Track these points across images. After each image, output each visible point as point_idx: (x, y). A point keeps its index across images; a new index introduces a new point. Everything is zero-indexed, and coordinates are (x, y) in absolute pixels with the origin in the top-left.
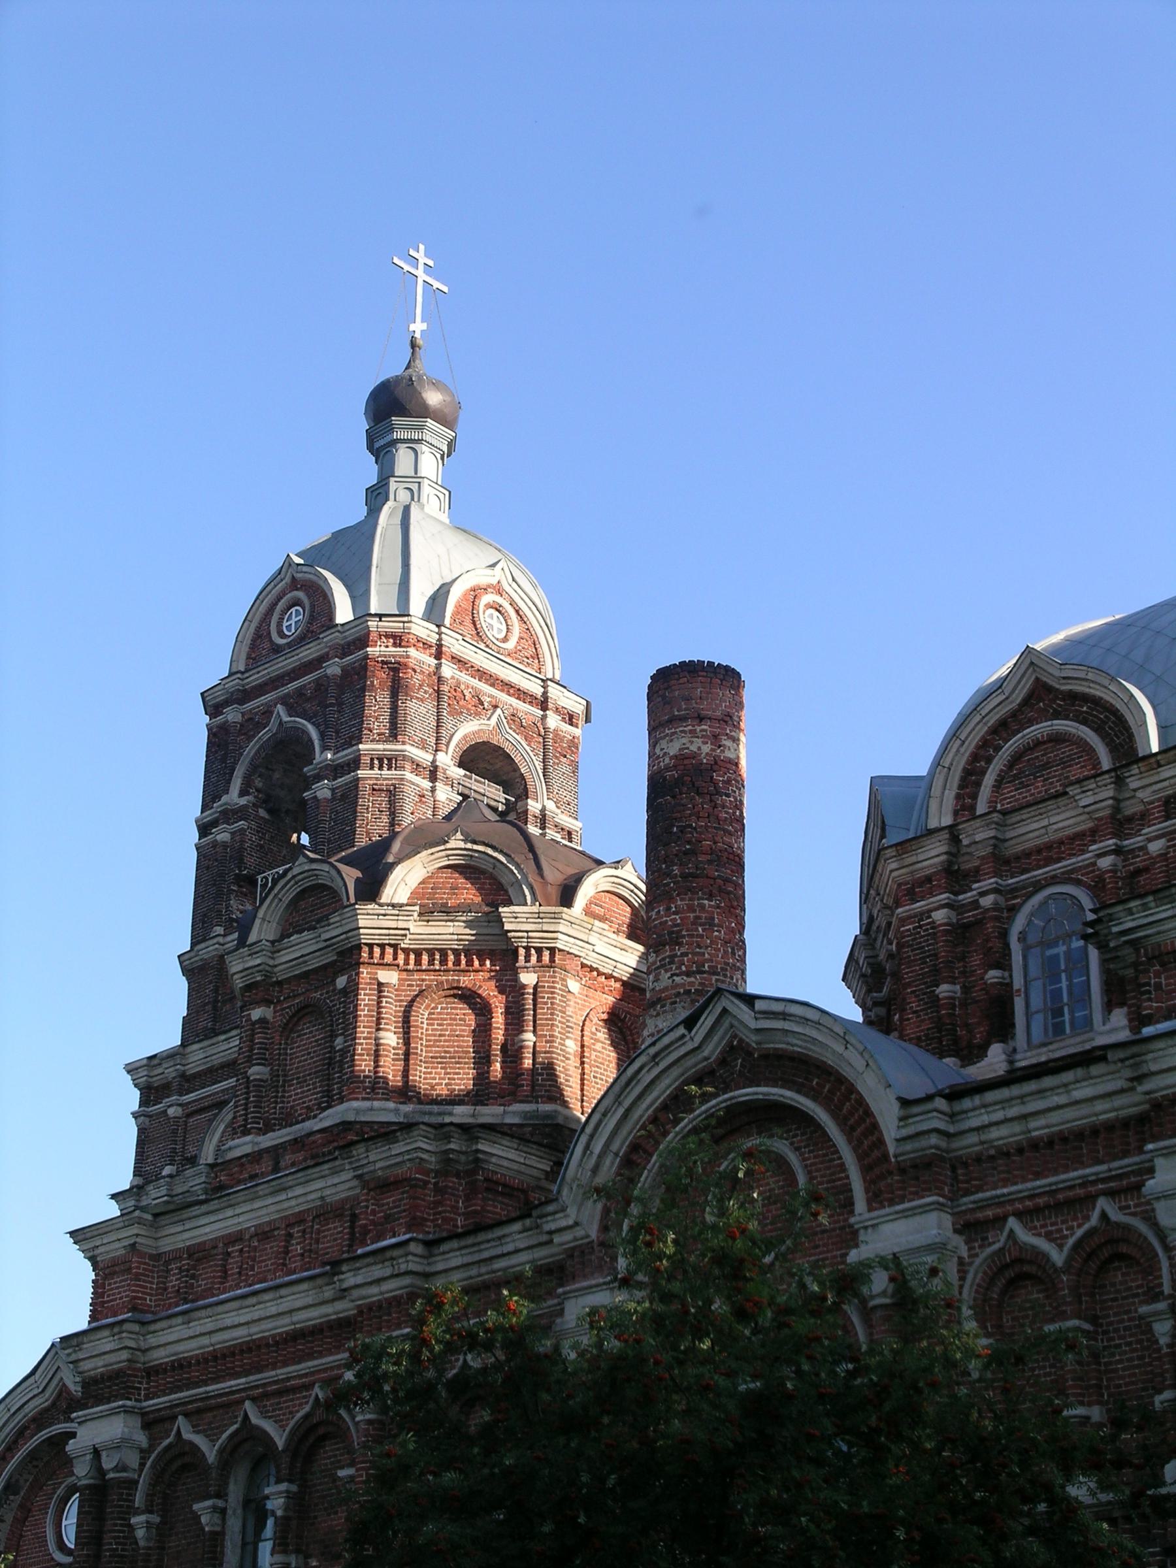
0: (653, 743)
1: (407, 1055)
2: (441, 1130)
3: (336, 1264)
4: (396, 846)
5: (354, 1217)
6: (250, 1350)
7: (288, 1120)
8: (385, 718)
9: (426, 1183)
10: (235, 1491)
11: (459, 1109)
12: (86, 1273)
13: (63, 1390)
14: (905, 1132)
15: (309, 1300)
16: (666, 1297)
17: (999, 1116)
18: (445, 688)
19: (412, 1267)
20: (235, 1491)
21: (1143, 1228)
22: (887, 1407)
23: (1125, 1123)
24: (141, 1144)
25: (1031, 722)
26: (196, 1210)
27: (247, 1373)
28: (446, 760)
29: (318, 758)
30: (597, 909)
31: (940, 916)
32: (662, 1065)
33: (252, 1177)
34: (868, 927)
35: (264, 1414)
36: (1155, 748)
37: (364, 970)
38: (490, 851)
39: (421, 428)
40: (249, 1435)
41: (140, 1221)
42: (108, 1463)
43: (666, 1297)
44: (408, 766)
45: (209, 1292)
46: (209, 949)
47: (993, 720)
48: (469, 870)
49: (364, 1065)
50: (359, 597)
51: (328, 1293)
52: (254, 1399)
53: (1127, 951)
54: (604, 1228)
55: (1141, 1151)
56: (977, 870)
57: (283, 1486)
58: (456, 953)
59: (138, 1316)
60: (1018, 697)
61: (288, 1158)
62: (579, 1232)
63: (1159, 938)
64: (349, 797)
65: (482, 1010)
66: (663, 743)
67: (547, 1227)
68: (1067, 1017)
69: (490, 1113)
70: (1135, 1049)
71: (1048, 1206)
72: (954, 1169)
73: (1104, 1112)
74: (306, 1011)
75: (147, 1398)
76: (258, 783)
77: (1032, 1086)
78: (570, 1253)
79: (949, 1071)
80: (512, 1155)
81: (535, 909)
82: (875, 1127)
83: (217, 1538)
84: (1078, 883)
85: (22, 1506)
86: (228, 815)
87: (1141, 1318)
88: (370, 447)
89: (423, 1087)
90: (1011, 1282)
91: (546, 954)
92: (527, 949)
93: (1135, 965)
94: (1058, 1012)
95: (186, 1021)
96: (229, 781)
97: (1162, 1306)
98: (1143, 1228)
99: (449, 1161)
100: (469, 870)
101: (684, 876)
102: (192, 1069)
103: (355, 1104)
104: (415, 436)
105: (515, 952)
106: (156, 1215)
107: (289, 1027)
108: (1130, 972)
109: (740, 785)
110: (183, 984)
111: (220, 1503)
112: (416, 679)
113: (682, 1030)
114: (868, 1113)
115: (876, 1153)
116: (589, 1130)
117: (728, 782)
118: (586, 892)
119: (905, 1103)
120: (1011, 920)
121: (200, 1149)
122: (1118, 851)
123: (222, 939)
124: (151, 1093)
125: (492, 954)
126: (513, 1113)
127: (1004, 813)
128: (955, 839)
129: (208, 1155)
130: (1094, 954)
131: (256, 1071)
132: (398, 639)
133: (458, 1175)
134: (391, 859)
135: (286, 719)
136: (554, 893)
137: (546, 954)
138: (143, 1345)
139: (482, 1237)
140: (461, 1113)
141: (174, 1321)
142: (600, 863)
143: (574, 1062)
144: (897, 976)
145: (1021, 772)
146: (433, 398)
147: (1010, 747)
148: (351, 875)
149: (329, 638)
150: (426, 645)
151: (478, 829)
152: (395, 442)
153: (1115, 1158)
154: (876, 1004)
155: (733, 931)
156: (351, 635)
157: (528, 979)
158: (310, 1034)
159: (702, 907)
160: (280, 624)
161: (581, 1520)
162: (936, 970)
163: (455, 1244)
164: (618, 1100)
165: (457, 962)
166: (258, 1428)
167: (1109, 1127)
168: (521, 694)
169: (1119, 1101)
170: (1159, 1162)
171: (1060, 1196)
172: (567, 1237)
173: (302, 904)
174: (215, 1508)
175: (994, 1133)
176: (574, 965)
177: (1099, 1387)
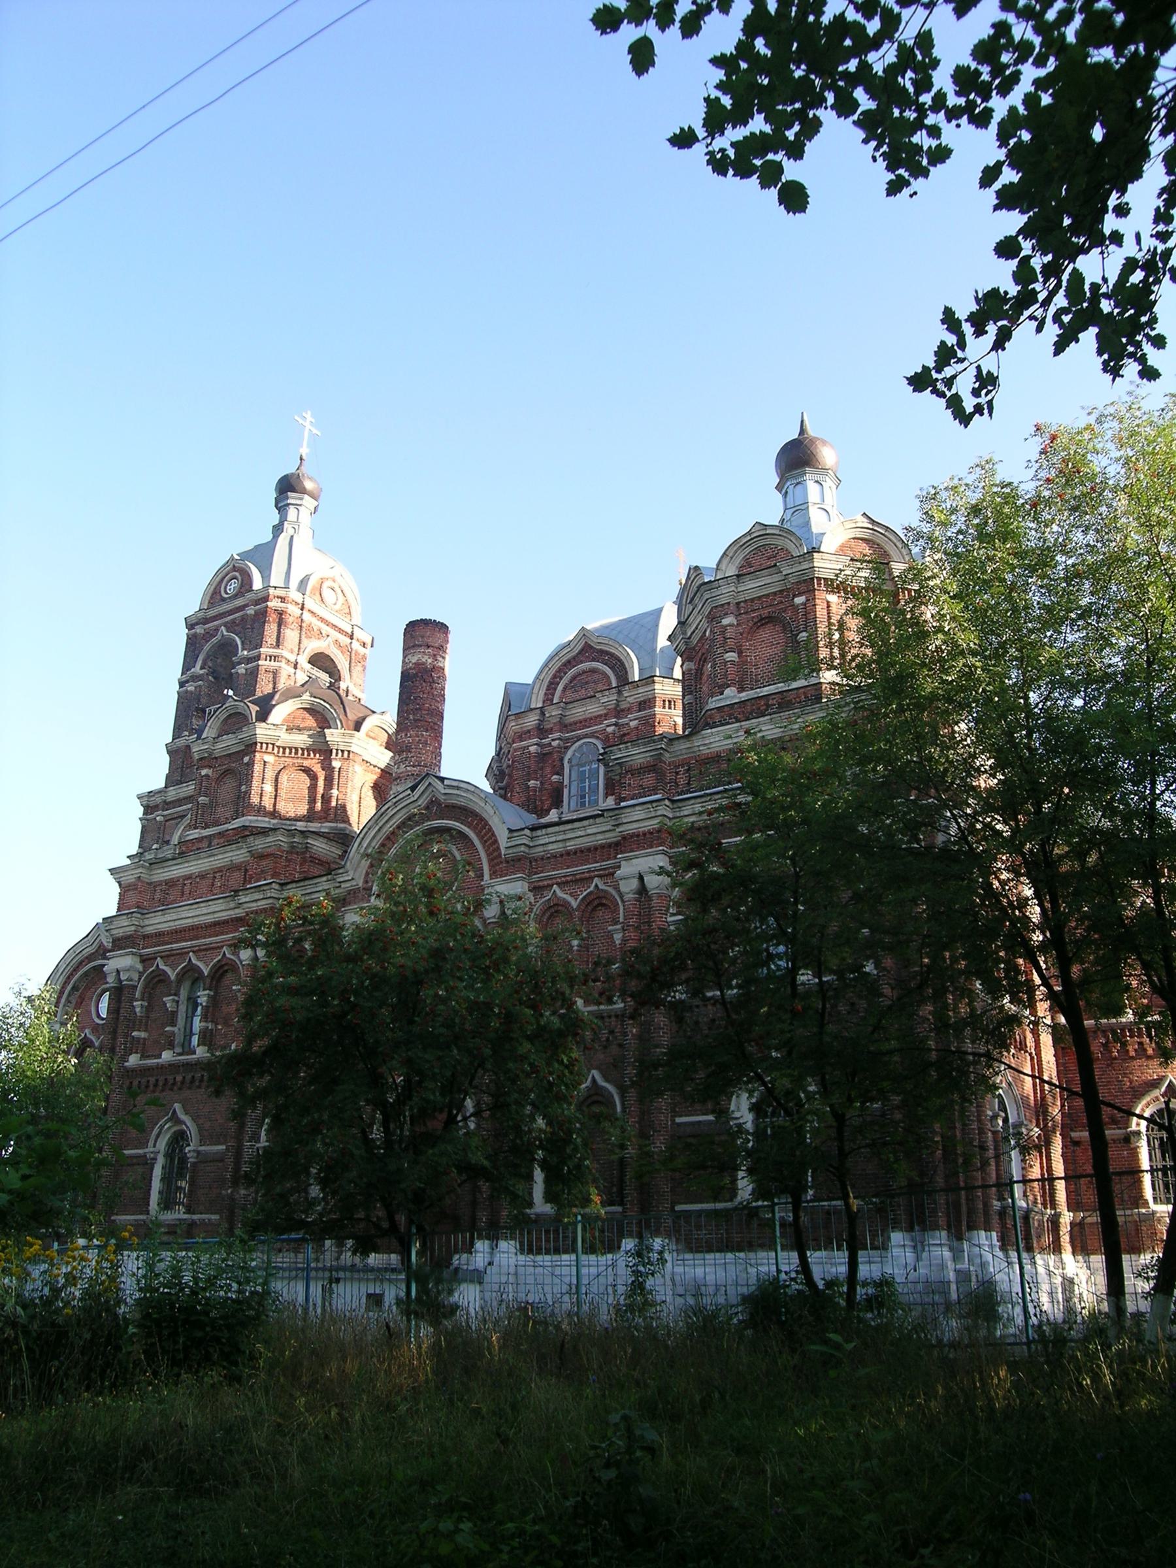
0: (405, 657)
1: (276, 796)
2: (291, 833)
3: (236, 891)
4: (277, 697)
5: (246, 870)
6: (193, 929)
7: (217, 823)
8: (274, 637)
9: (282, 856)
10: (184, 993)
11: (299, 823)
12: (116, 889)
13: (101, 945)
14: (509, 844)
15: (223, 908)
16: (397, 904)
17: (553, 839)
18: (304, 625)
19: (273, 895)
20: (184, 993)
21: (614, 892)
22: (494, 957)
23: (610, 845)
24: (142, 832)
25: (582, 662)
26: (170, 863)
27: (191, 940)
28: (303, 661)
29: (240, 653)
30: (372, 734)
31: (533, 749)
32: (398, 808)
33: (198, 849)
34: (498, 754)
35: (199, 959)
36: (637, 678)
37: (257, 754)
38: (322, 702)
39: (301, 499)
40: (191, 969)
41: (143, 866)
42: (123, 977)
43: (397, 904)
44: (284, 660)
45: (175, 901)
46: (181, 742)
47: (564, 660)
48: (311, 711)
49: (255, 800)
50: (266, 576)
51: (232, 905)
52: (194, 952)
53: (617, 767)
54: (366, 882)
55: (615, 858)
56: (552, 729)
57: (207, 992)
58: (303, 750)
59: (140, 911)
60: (579, 648)
61: (215, 842)
62: (354, 883)
63: (631, 763)
64: (254, 674)
65: (314, 778)
66: (409, 657)
67: (339, 880)
68: (587, 799)
69: (314, 826)
70: (617, 812)
71: (572, 881)
72: (531, 862)
73: (601, 840)
74: (227, 772)
75: (143, 949)
76: (210, 664)
77: (569, 826)
78: (349, 893)
79: (532, 819)
80: (323, 846)
81: (343, 731)
82: (496, 841)
83: (174, 1014)
84: (597, 738)
85: (80, 996)
86: (194, 678)
87: (609, 932)
88: (276, 506)
89: (283, 812)
90: (552, 915)
91: (346, 753)
92: (337, 750)
93: (620, 774)
94: (583, 797)
95: (168, 776)
96: (195, 662)
97: (619, 927)
98: (614, 892)
99: (293, 847)
100: (311, 711)
101: (415, 720)
102: (169, 799)
103: (249, 818)
104: (299, 502)
105: (331, 751)
106: (151, 864)
107: (220, 779)
108: (617, 778)
109: (444, 679)
110: (167, 758)
111: (176, 998)
112: (290, 620)
113: (409, 792)
114: (493, 835)
115: (496, 854)
116: (361, 836)
117: (439, 677)
118: (365, 727)
119: (511, 831)
120: (565, 753)
121: (171, 837)
122: (616, 724)
123: (187, 738)
124: (148, 809)
125: (320, 752)
126: (326, 827)
127: (566, 703)
128: (543, 714)
129: (175, 840)
130: (602, 769)
131: (202, 799)
132: (283, 599)
133: (297, 853)
134: (274, 703)
135: (225, 633)
136: (352, 725)
137: (346, 753)
138: (142, 924)
139: (307, 882)
140: (300, 825)
141: (157, 914)
142: (374, 712)
143: (356, 805)
144: (510, 776)
145: (576, 685)
146: (309, 485)
147: (572, 672)
148: (254, 709)
149: (249, 596)
150: (297, 604)
151: (317, 692)
152: (288, 504)
153: (604, 861)
154: (500, 788)
155: (436, 748)
156: (261, 595)
157: (336, 764)
158: (229, 784)
159: (423, 735)
160: (226, 588)
161: (352, 999)
162: (529, 774)
163: (294, 885)
164: (376, 822)
165: (303, 754)
166: (196, 965)
167: (602, 847)
168: (341, 631)
169: (608, 835)
170: (623, 863)
171: (578, 877)
172: (348, 885)
173: (229, 721)
174: (173, 1000)
175: (551, 847)
176: (359, 759)
177: (588, 961)
